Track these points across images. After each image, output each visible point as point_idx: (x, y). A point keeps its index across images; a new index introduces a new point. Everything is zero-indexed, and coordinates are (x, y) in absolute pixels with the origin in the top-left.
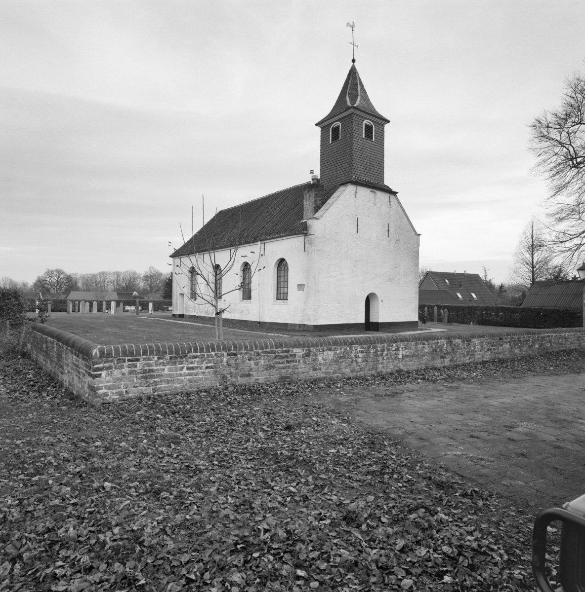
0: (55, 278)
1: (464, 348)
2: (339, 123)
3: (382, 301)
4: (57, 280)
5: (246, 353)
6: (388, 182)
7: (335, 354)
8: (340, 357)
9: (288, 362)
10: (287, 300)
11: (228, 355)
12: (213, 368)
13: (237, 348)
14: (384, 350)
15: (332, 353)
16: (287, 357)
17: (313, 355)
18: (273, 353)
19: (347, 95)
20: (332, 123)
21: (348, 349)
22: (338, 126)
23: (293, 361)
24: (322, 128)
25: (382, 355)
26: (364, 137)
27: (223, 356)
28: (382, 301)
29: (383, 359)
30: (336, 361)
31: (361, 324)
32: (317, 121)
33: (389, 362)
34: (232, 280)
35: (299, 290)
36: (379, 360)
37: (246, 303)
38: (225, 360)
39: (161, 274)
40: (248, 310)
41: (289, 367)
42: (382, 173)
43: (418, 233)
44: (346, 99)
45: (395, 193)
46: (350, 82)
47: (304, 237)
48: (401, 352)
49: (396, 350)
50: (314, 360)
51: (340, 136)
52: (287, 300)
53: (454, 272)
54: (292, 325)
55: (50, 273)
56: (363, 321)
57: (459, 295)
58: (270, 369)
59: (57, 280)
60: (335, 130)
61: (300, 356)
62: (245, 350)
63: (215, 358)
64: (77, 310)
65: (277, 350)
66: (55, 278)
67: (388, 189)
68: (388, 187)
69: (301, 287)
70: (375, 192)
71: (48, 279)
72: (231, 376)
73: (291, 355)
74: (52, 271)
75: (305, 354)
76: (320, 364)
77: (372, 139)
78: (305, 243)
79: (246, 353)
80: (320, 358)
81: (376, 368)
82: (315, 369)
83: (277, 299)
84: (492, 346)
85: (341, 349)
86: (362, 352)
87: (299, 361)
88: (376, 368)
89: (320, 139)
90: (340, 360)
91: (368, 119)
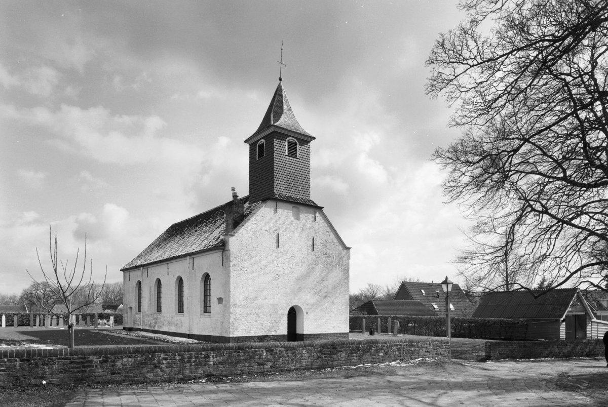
0: (42, 291)
1: (288, 356)
2: (263, 141)
3: (307, 313)
4: (44, 293)
5: (40, 359)
6: (315, 197)
7: (136, 360)
8: (142, 364)
9: (84, 367)
10: (210, 313)
11: (21, 361)
12: (5, 371)
13: (30, 355)
14: (191, 358)
15: (133, 360)
16: (83, 363)
17: (111, 362)
18: (68, 360)
19: (272, 114)
20: (258, 141)
21: (150, 356)
22: (263, 144)
23: (89, 366)
24: (250, 145)
25: (189, 361)
26: (287, 154)
27: (16, 361)
28: (307, 313)
29: (191, 365)
30: (137, 367)
31: (284, 335)
32: (245, 139)
33: (198, 368)
34: (193, 292)
35: (219, 303)
36: (186, 367)
37: (179, 317)
38: (18, 364)
39: (15, 297)
40: (181, 322)
41: (85, 371)
42: (308, 186)
43: (348, 246)
44: (270, 118)
45: (320, 208)
46: (276, 100)
47: (222, 252)
48: (211, 359)
49: (205, 357)
50: (113, 366)
51: (265, 153)
52: (210, 313)
53: (431, 282)
54: (214, 337)
55: (36, 286)
56: (283, 330)
57: (436, 307)
58: (65, 373)
59: (44, 293)
60: (261, 147)
61: (96, 362)
62: (38, 356)
63: (7, 363)
64: (42, 324)
65: (72, 357)
66: (42, 291)
67: (313, 204)
68: (313, 202)
69: (220, 300)
70: (298, 208)
71: (34, 292)
72: (25, 378)
73: (87, 362)
74: (38, 284)
75: (103, 360)
76: (119, 369)
77: (297, 156)
78: (223, 258)
79: (40, 359)
80: (118, 364)
81: (183, 373)
82: (113, 374)
83: (204, 312)
84: (323, 354)
85: (142, 356)
86: (166, 359)
87: (96, 366)
88: (183, 373)
89: (249, 156)
90: (141, 366)
91: (291, 136)
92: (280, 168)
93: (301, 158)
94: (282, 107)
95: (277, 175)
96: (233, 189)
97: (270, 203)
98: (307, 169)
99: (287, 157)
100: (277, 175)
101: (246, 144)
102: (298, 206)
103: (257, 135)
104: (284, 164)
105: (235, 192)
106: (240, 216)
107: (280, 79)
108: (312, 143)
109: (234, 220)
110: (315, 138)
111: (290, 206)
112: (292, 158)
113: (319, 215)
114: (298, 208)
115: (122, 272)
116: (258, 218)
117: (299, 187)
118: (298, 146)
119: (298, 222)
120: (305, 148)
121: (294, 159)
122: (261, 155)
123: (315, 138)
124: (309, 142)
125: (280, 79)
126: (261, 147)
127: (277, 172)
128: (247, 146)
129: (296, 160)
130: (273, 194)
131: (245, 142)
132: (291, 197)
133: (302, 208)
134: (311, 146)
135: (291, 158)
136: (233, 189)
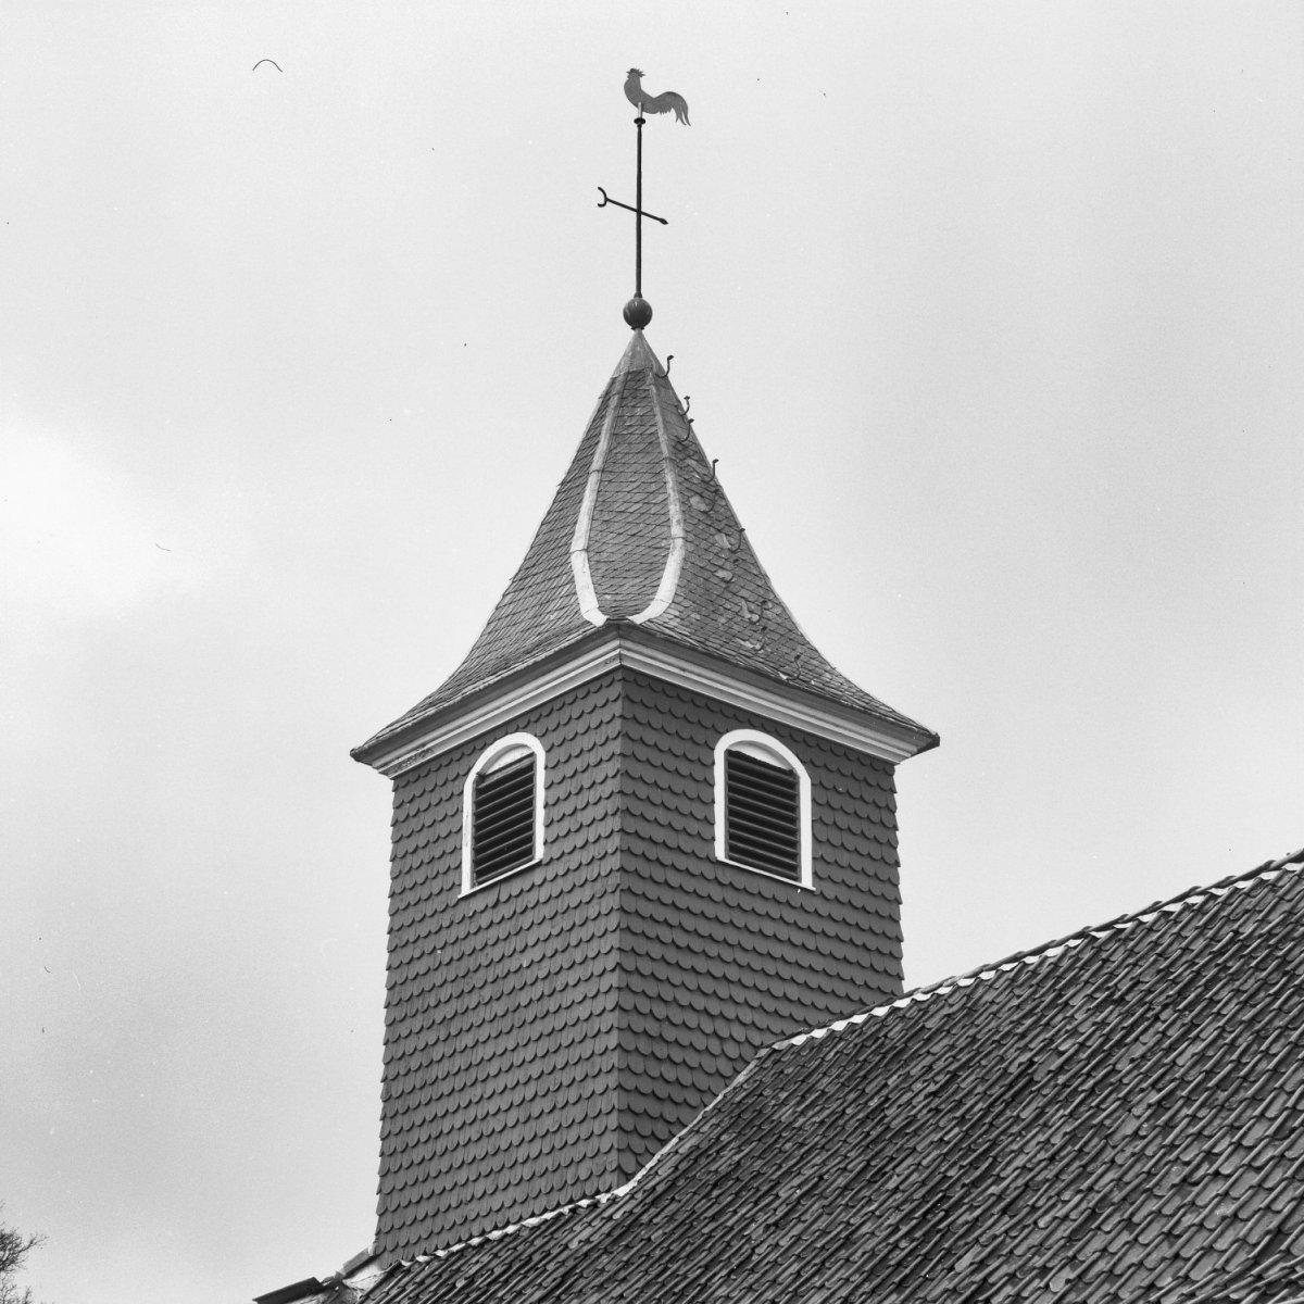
24: (401, 783)
110: (932, 741)
123: (932, 741)
125: (638, 316)
131: (362, 755)
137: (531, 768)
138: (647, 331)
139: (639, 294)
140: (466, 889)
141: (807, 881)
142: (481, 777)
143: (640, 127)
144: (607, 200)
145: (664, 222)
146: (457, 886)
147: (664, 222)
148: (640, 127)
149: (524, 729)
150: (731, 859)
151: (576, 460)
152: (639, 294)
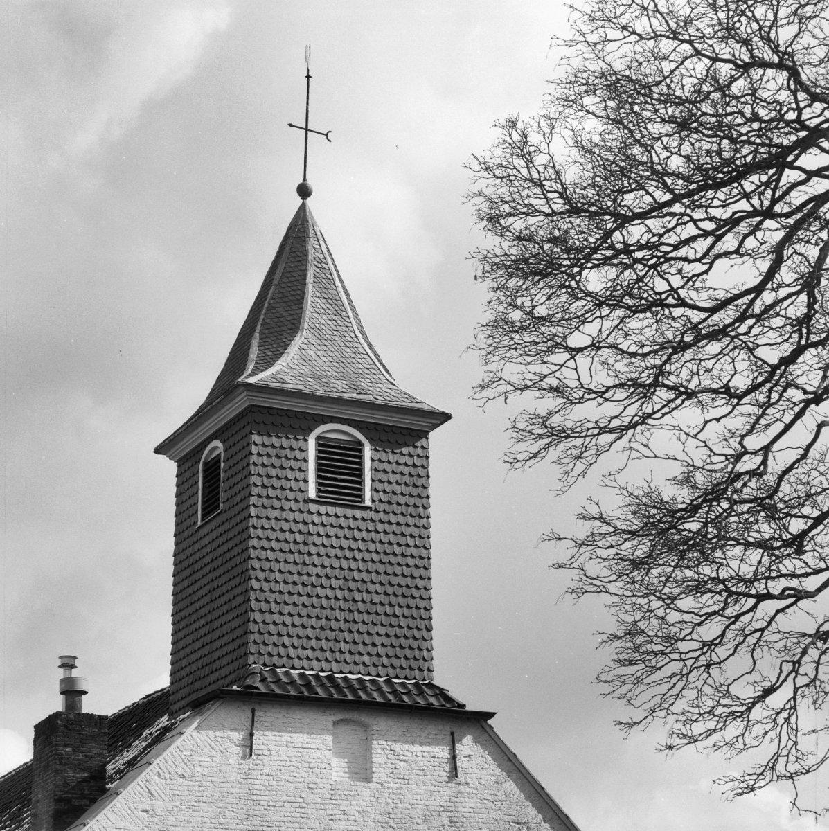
24: (180, 463)
26: (312, 494)
60: (212, 469)
70: (366, 727)
77: (362, 497)
92: (281, 557)
93: (381, 507)
94: (299, 300)
95: (266, 586)
96: (68, 664)
97: (217, 713)
98: (415, 552)
99: (313, 508)
100: (266, 586)
101: (163, 458)
102: (364, 718)
103: (221, 405)
104: (299, 538)
105: (75, 673)
106: (85, 780)
107: (304, 191)
108: (437, 439)
109: (59, 800)
110: (446, 417)
111: (328, 719)
112: (339, 511)
113: (479, 750)
114: (366, 727)
115: (62, 670)
116: (157, 784)
117: (373, 630)
118: (368, 452)
119: (364, 789)
120: (402, 460)
121: (350, 512)
122: (211, 504)
123: (446, 417)
124: (424, 434)
125: (304, 191)
126: (212, 469)
127: (261, 575)
128: (168, 467)
129: (358, 514)
130: (244, 671)
131: (158, 450)
132: (331, 678)
133: (380, 723)
134: (431, 452)
135: (331, 510)
136: (68, 664)
137: (219, 461)
138: (309, 201)
139: (305, 180)
140: (199, 523)
141: (368, 503)
142: (205, 464)
143: (308, 80)
144: (327, 135)
145: (291, 125)
146: (195, 523)
147: (291, 125)
148: (308, 80)
149: (216, 439)
150: (319, 497)
151: (266, 280)
152: (305, 180)
